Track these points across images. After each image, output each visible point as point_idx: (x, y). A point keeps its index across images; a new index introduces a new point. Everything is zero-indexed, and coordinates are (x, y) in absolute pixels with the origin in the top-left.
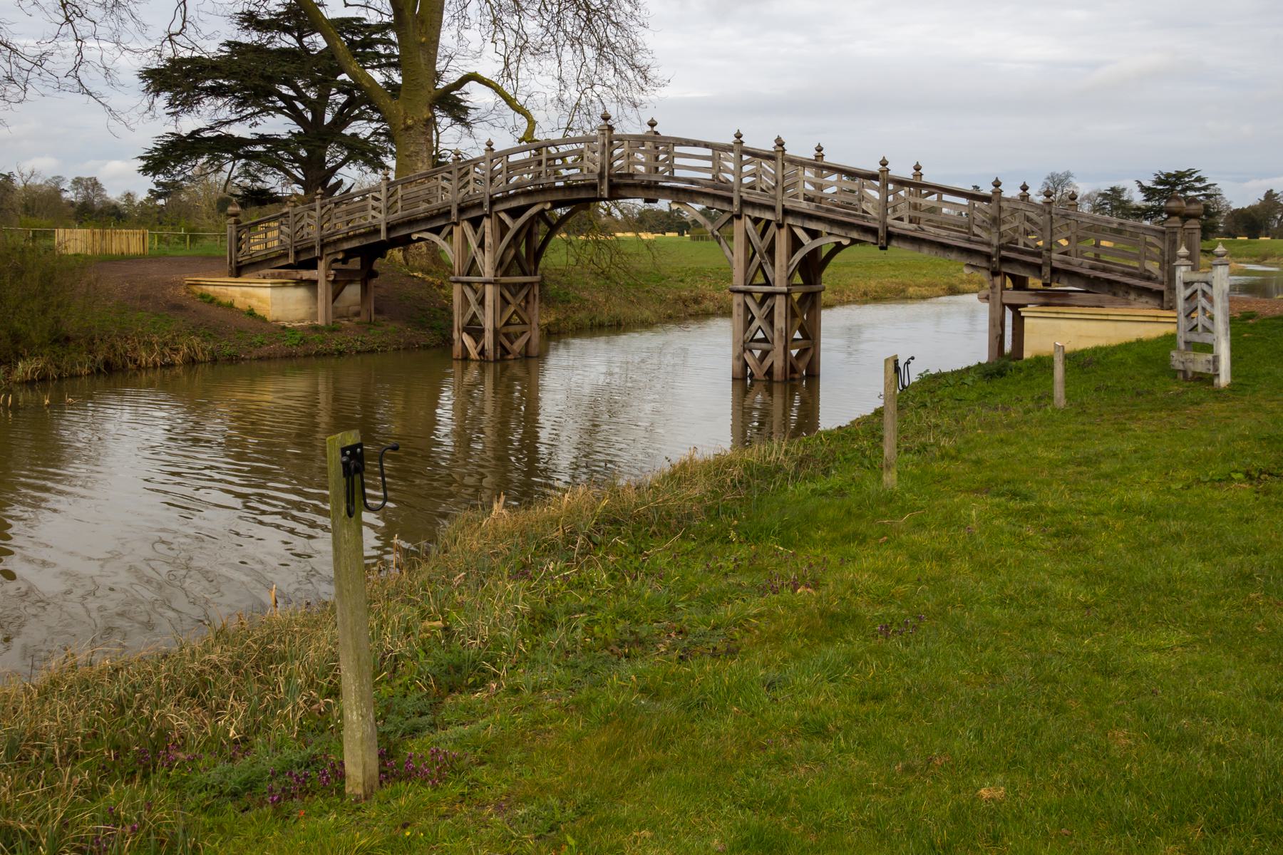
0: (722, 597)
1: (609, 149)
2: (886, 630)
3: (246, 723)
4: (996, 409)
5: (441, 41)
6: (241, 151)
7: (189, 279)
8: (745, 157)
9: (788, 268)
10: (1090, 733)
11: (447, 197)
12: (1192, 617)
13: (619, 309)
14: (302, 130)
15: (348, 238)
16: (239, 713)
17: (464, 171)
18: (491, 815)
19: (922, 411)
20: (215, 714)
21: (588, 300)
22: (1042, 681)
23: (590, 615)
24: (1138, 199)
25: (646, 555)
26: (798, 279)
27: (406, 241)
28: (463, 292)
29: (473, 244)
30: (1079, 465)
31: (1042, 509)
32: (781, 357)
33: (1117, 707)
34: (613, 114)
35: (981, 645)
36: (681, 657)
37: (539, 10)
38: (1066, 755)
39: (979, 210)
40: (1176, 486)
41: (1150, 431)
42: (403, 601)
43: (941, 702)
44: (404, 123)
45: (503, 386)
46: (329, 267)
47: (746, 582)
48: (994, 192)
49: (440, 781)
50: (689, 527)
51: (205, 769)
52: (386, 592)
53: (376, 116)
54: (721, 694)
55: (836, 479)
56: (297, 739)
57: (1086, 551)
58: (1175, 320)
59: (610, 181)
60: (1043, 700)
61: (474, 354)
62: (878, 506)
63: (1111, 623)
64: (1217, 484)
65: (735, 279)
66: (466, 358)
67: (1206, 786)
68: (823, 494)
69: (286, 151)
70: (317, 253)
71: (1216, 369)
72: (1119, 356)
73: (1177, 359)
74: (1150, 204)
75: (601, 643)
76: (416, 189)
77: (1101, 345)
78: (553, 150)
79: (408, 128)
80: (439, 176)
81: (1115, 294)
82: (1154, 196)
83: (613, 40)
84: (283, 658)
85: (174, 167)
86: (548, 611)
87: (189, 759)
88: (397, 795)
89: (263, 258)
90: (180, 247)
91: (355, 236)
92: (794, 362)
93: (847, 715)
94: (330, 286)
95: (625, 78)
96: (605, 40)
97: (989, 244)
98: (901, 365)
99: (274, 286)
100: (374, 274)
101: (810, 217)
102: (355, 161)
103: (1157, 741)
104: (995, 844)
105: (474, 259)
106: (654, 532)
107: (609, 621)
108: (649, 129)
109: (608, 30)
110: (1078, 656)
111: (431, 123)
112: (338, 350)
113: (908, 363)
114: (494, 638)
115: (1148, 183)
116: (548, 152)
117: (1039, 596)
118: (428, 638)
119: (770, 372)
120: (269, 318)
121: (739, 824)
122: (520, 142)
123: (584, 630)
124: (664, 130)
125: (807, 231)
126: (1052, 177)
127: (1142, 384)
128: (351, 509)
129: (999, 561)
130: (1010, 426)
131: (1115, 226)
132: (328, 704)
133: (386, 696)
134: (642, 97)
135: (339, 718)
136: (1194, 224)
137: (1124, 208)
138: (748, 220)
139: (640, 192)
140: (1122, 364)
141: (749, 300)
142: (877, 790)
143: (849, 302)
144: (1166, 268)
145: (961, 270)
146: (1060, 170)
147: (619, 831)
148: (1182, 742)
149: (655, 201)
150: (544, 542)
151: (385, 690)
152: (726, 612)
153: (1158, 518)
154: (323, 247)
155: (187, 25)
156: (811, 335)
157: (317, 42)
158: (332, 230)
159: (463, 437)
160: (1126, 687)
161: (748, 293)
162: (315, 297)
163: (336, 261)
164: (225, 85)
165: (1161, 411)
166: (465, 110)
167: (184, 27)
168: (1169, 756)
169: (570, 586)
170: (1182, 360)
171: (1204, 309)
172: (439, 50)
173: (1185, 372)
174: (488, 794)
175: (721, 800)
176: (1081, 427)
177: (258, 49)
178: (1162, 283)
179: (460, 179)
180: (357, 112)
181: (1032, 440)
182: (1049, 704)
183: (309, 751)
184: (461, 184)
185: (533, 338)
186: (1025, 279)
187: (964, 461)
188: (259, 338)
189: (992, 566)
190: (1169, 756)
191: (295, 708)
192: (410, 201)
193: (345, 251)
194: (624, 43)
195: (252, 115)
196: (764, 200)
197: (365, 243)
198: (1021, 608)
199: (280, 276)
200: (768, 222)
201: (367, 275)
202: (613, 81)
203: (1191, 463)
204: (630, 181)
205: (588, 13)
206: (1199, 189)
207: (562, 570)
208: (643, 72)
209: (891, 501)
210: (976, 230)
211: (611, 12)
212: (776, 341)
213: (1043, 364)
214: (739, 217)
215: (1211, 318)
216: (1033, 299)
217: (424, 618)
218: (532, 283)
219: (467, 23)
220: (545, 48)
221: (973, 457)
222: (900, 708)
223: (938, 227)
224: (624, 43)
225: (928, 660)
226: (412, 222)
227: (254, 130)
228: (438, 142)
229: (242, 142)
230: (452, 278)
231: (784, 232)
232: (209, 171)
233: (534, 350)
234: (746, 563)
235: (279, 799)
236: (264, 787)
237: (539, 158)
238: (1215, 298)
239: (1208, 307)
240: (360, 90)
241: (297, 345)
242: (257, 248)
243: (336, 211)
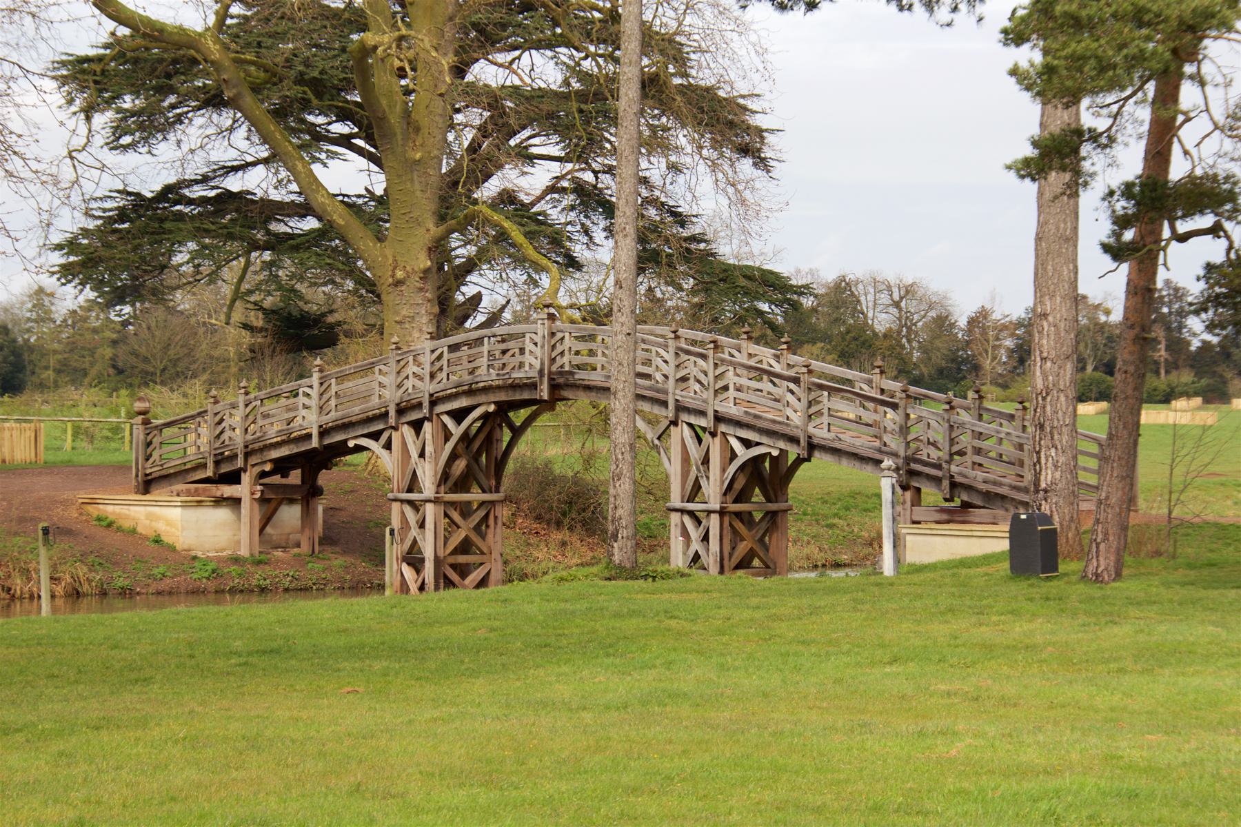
1: (549, 342)
7: (83, 495)
28: (403, 513)
29: (414, 454)
59: (551, 379)
70: (240, 463)
79: (398, 283)
90: (113, 445)
94: (256, 506)
99: (185, 505)
105: (415, 471)
112: (259, 586)
120: (179, 547)
138: (685, 426)
154: (247, 455)
158: (258, 434)
162: (239, 519)
188: (162, 569)
197: (296, 450)
201: (310, 492)
212: (711, 568)
214: (674, 423)
226: (346, 426)
230: (390, 496)
241: (208, 579)
243: (262, 410)
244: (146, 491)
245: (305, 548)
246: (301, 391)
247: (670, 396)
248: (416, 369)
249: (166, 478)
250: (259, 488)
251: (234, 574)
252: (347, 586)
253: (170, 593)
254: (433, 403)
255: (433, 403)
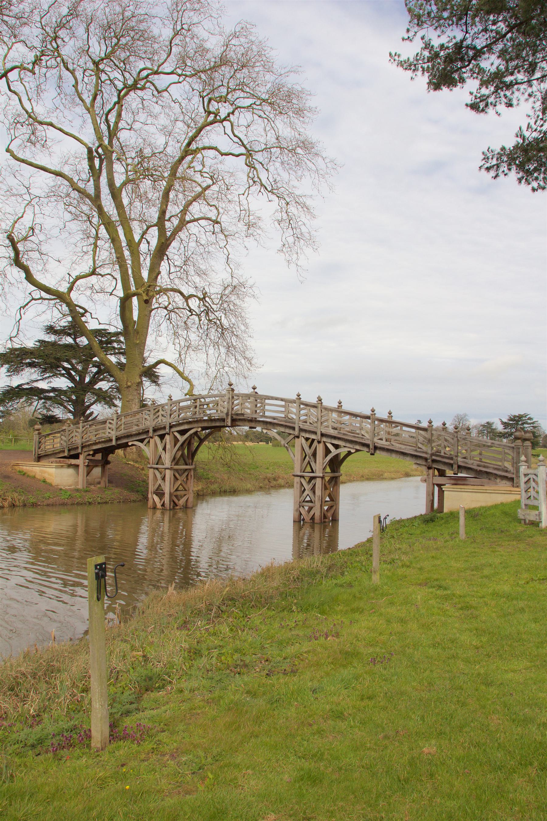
0: (289, 642)
2: (374, 661)
3: (39, 706)
4: (430, 539)
5: (147, 342)
6: (42, 396)
8: (302, 406)
9: (323, 464)
10: (479, 717)
11: (148, 423)
12: (530, 653)
13: (235, 483)
14: (73, 386)
15: (96, 444)
16: (36, 700)
17: (156, 410)
18: (168, 760)
19: (392, 541)
20: (24, 700)
21: (218, 478)
22: (454, 689)
23: (219, 650)
24: (500, 428)
25: (249, 618)
26: (328, 470)
27: (126, 446)
28: (154, 473)
29: (160, 448)
30: (472, 570)
31: (454, 595)
32: (319, 510)
33: (493, 703)
34: (233, 382)
35: (423, 669)
36: (267, 674)
37: (197, 328)
38: (467, 729)
39: (421, 435)
40: (521, 582)
41: (508, 552)
42: (122, 640)
43: (402, 700)
44: (127, 384)
45: (173, 520)
46: (86, 459)
47: (301, 633)
48: (429, 426)
49: (142, 741)
50: (271, 603)
51: (17, 731)
52: (112, 635)
53: (112, 379)
54: (289, 695)
55: (347, 578)
56: (66, 716)
57: (476, 617)
58: (520, 493)
59: (232, 417)
60: (455, 699)
61: (159, 505)
62: (370, 593)
63: (490, 657)
64: (542, 581)
65: (295, 469)
66: (155, 508)
67: (538, 746)
68: (341, 586)
69: (65, 396)
70: (80, 450)
71: (540, 519)
72: (492, 511)
73: (521, 514)
74: (506, 431)
75: (226, 666)
76: (131, 419)
77: (483, 505)
78: (202, 400)
79: (128, 387)
80: (144, 412)
81: (490, 479)
82: (508, 426)
83: (235, 344)
84: (59, 671)
85: (8, 403)
86: (198, 648)
87: (9, 725)
88: (118, 748)
89: (52, 452)
90: (9, 444)
91: (99, 443)
92: (326, 513)
93: (354, 707)
94: (85, 468)
95: (240, 363)
96: (230, 344)
97: (426, 453)
98: (382, 519)
99: (57, 467)
100: (108, 463)
101: (335, 438)
102: (100, 402)
103: (513, 721)
104: (431, 778)
106: (253, 606)
107: (230, 654)
108: (253, 390)
109: (232, 339)
110: (473, 675)
111: (140, 384)
112: (88, 502)
113: (385, 518)
114: (169, 662)
115: (505, 420)
116: (201, 401)
117: (453, 642)
118: (135, 661)
119: (313, 518)
121: (298, 767)
122: (186, 395)
123: (217, 658)
124: (260, 391)
125: (333, 445)
126: (457, 416)
127: (504, 526)
128: (99, 596)
129: (432, 623)
130: (437, 549)
131: (489, 444)
132: (82, 696)
133: (113, 693)
134: (249, 373)
135: (88, 704)
136: (528, 443)
137: (493, 432)
139: (247, 423)
140: (493, 515)
141: (302, 480)
142: (370, 748)
143: (354, 481)
144: (515, 466)
145: (409, 464)
146: (461, 413)
147: (235, 770)
148: (526, 721)
149: (255, 428)
150: (196, 609)
151: (112, 689)
152: (290, 650)
153: (512, 599)
154: (82, 447)
155: (20, 332)
156: (334, 499)
157: (83, 341)
158: (88, 439)
159: (152, 547)
160: (497, 692)
161: (303, 477)
162: (78, 474)
163: (89, 455)
164: (35, 362)
165: (513, 540)
166: (157, 377)
167: (18, 334)
168: (519, 729)
169: (210, 634)
170: (523, 514)
171: (534, 488)
172: (146, 347)
173: (525, 520)
174: (166, 749)
175: (289, 754)
176: (473, 550)
177: (54, 344)
178: (513, 474)
179: (154, 414)
180: (102, 377)
181: (448, 557)
182: (458, 701)
183: (72, 723)
184: (155, 417)
185: (190, 498)
186: (444, 471)
187: (414, 568)
189: (428, 626)
190: (519, 729)
191: (64, 699)
192: (129, 425)
193: (94, 450)
194: (240, 346)
195: (49, 377)
196: (311, 428)
197: (104, 446)
198: (444, 649)
199: (60, 462)
200: (313, 440)
201: (105, 463)
202: (235, 365)
203: (529, 570)
204: (242, 417)
205: (222, 330)
206: (530, 424)
207: (204, 625)
208: (249, 360)
209: (376, 590)
210: (420, 445)
211: (234, 329)
213: (454, 516)
214: (298, 437)
215: (537, 492)
216: (449, 481)
217: (133, 650)
218: (190, 469)
219: (160, 334)
220: (200, 347)
221: (418, 566)
222: (381, 704)
223: (400, 444)
224: (240, 346)
225: (396, 677)
227: (50, 385)
228: (143, 394)
229: (43, 391)
230: (149, 466)
231: (321, 445)
232: (25, 405)
233: (190, 504)
234: (301, 623)
235: (57, 749)
236: (48, 742)
237: (195, 404)
238: (539, 482)
239: (536, 487)
240: (103, 365)
241: (68, 499)
242: (49, 447)
243: (90, 429)
244: (38, 461)
245: (102, 485)
246: (108, 421)
247: (296, 424)
248: (162, 413)
249: (47, 456)
250: (87, 461)
251: (78, 496)
252: (121, 501)
253: (52, 505)
254: (171, 427)
255: (171, 427)
